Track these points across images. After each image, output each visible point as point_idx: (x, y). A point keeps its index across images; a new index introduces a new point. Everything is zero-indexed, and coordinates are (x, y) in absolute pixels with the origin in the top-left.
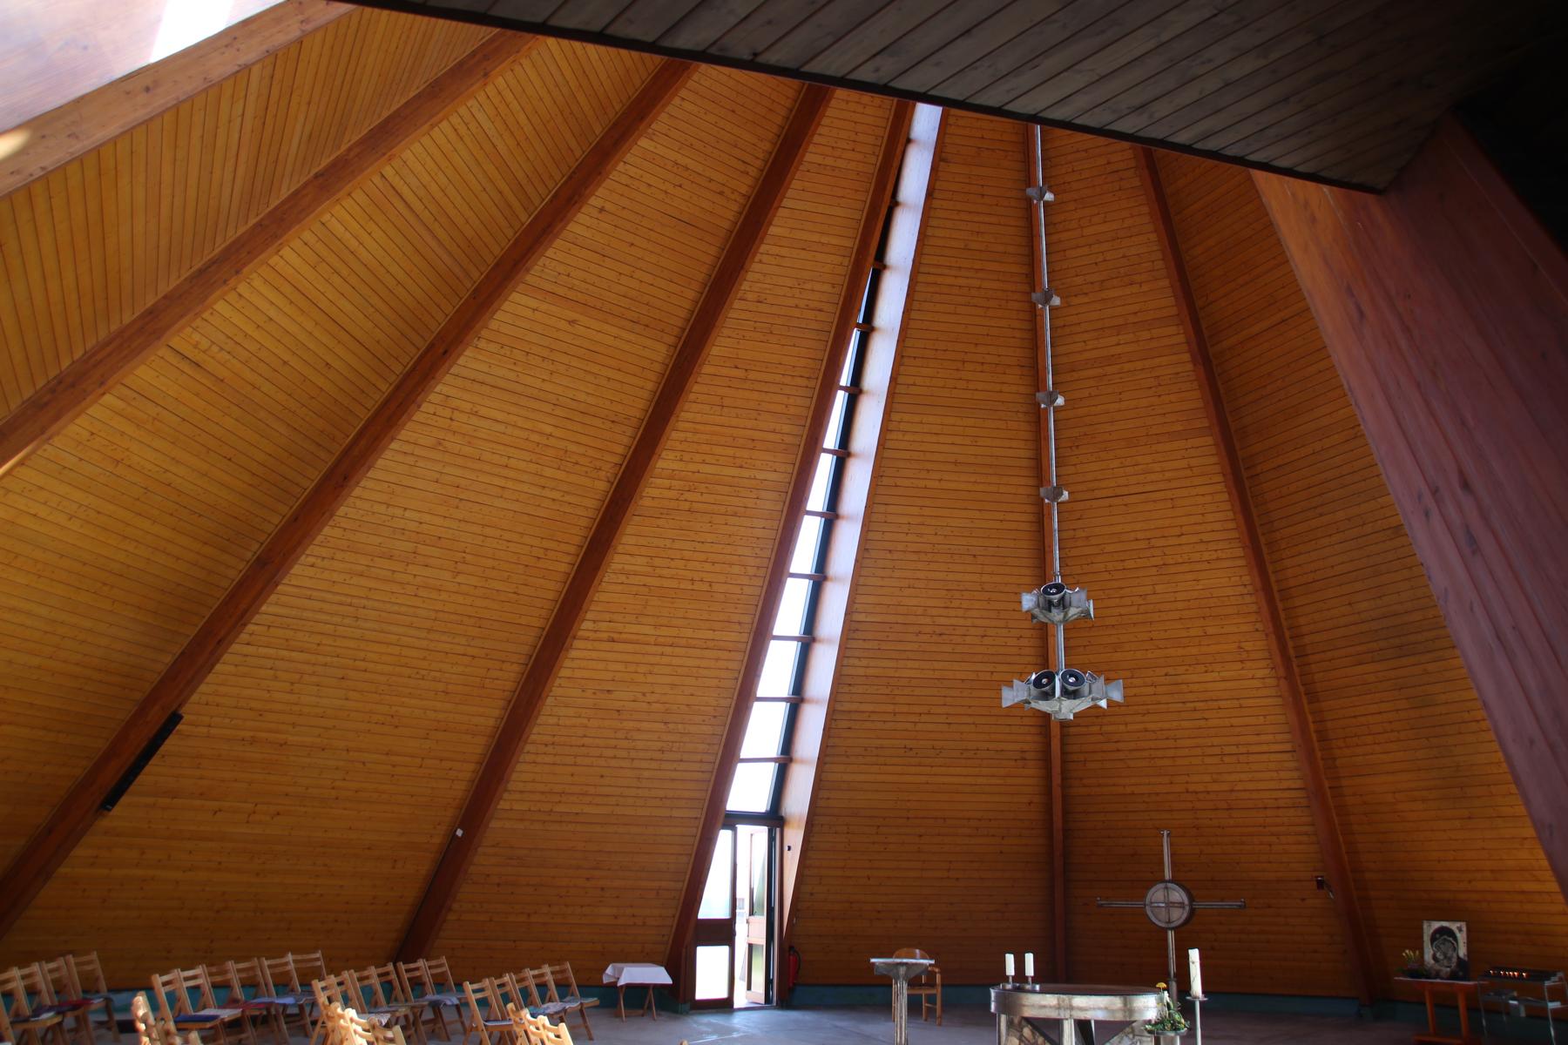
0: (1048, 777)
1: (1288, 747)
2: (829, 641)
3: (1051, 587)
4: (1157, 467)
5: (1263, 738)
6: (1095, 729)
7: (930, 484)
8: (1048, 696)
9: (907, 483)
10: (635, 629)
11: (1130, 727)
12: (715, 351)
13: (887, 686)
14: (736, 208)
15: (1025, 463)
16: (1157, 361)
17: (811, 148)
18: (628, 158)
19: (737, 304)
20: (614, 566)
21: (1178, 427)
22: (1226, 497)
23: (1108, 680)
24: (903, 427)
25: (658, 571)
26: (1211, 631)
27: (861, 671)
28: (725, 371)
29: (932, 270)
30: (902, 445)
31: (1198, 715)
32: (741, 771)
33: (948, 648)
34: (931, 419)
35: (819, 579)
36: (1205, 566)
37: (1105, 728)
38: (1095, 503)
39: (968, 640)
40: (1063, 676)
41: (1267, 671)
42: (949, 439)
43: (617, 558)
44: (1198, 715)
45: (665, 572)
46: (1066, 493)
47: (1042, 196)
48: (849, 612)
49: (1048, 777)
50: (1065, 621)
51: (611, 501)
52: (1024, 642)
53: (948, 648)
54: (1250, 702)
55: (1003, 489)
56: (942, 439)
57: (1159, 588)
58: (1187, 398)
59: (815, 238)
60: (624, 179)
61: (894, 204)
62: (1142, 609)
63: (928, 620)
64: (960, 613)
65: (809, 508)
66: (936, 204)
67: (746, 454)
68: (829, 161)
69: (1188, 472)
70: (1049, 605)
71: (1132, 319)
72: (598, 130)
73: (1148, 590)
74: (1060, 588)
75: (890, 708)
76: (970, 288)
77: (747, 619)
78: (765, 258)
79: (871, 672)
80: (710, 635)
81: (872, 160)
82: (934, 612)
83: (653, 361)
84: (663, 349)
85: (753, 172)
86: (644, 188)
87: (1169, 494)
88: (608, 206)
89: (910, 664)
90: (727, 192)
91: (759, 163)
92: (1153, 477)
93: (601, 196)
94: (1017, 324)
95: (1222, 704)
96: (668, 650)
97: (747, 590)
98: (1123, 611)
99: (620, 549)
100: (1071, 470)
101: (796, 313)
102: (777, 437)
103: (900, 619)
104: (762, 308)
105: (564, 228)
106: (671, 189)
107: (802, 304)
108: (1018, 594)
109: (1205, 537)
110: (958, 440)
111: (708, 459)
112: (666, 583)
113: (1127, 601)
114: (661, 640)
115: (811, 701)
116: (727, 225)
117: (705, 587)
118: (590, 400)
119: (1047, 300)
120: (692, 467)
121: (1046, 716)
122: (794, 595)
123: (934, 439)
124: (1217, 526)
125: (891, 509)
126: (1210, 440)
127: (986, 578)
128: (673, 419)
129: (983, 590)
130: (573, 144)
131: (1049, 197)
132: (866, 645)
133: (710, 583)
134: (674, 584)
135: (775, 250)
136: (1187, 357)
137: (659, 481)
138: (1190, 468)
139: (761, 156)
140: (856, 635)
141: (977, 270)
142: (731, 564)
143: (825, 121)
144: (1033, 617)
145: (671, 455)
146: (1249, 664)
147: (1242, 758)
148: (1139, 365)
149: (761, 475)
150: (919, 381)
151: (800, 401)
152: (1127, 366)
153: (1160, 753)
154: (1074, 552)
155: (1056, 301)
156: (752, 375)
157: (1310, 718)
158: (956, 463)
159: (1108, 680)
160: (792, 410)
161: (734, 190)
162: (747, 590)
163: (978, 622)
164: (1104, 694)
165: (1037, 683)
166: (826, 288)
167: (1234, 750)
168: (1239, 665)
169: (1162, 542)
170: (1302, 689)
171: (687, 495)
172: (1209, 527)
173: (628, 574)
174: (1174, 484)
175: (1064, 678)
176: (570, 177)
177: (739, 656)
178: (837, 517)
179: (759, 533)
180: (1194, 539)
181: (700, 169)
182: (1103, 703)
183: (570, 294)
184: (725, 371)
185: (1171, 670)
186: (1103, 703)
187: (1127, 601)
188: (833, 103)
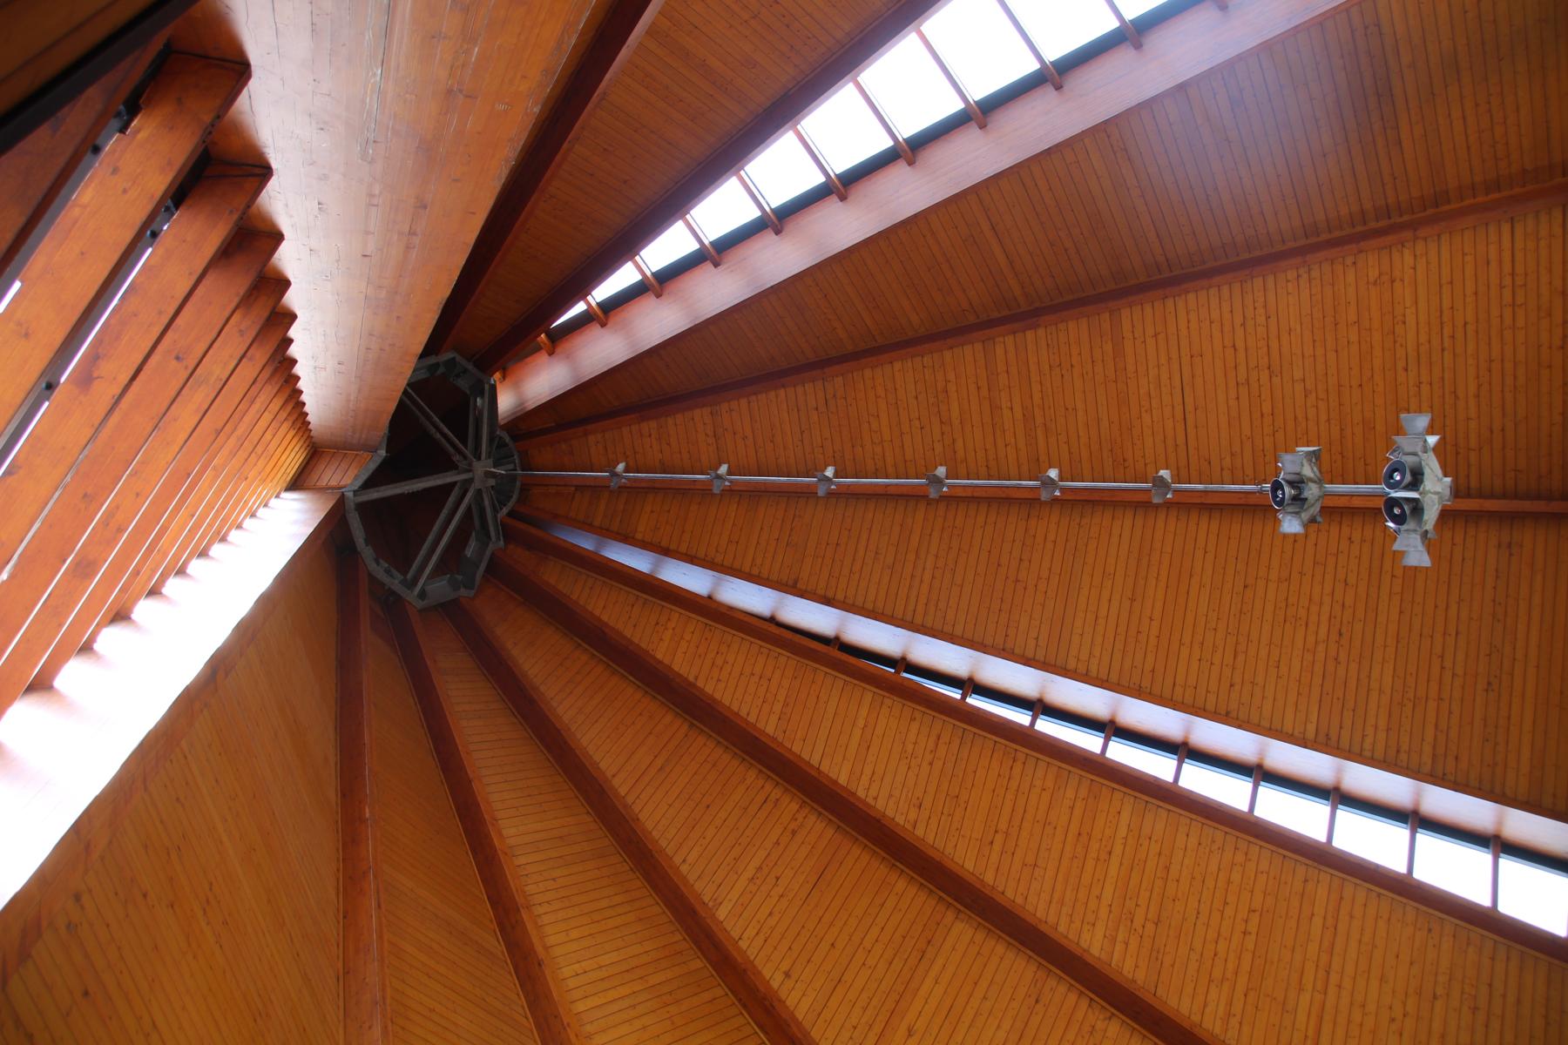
0: (1536, 517)
1: (1506, 228)
2: (1339, 771)
3: (1275, 496)
5: (1493, 255)
6: (1473, 457)
7: (1155, 632)
8: (1417, 508)
9: (1150, 658)
10: (1302, 1017)
11: (1473, 413)
12: (969, 865)
13: (1402, 705)
14: (813, 818)
15: (1139, 522)
16: (1033, 368)
17: (761, 725)
18: (735, 934)
19: (920, 832)
20: (1217, 1031)
21: (1108, 347)
22: (1191, 296)
23: (1399, 431)
25: (1229, 975)
26: (1353, 317)
27: (1382, 736)
28: (994, 857)
29: (911, 608)
30: (1106, 659)
31: (1459, 335)
32: (1422, 874)
33: (1358, 626)
34: (1078, 623)
35: (1183, 750)
36: (1273, 320)
37: (1473, 444)
39: (1349, 601)
40: (1391, 487)
41: (1406, 252)
43: (1207, 1024)
44: (1459, 335)
45: (1231, 966)
46: (1163, 473)
48: (1304, 743)
49: (1536, 517)
51: (1134, 1019)
52: (1357, 536)
53: (1358, 626)
54: (1446, 272)
56: (1103, 613)
57: (1298, 375)
58: (1076, 332)
59: (857, 733)
61: (772, 620)
62: (1322, 395)
63: (1321, 648)
64: (1314, 609)
65: (1098, 751)
66: (840, 596)
67: (1095, 846)
68: (778, 707)
69: (1162, 337)
70: (1298, 500)
71: (984, 392)
72: (698, 964)
73: (1299, 387)
74: (1277, 486)
75: (1432, 705)
76: (935, 567)
77: (1301, 870)
78: (873, 792)
79: (1382, 723)
80: (1318, 921)
81: (783, 660)
82: (1311, 639)
83: (972, 941)
84: (960, 926)
85: (777, 793)
86: (772, 921)
87: (1186, 360)
88: (785, 966)
90: (793, 826)
91: (769, 787)
92: (1165, 376)
93: (772, 974)
94: (981, 519)
95: (1446, 303)
96: (1334, 978)
97: (1264, 866)
98: (1323, 417)
99: (1196, 1018)
101: (938, 765)
102: (1079, 805)
103: (1317, 680)
105: (799, 1024)
106: (780, 890)
107: (929, 757)
108: (1285, 536)
109: (1238, 320)
110: (1106, 594)
111: (1096, 892)
112: (1246, 966)
113: (1312, 413)
114: (1319, 985)
115: (1417, 803)
116: (830, 831)
117: (1255, 918)
118: (1006, 1026)
119: (938, 481)
120: (1104, 911)
121: (1445, 515)
122: (1200, 781)
123: (1101, 621)
124: (1226, 307)
125: (1180, 680)
126: (1125, 313)
127: (1274, 575)
128: (1043, 928)
129: (1289, 579)
130: (706, 996)
131: (829, 472)
132: (1347, 722)
134: (1247, 957)
135: (865, 779)
136: (1030, 334)
137: (1116, 956)
139: (761, 782)
140: (1334, 738)
142: (1229, 882)
143: (735, 708)
144: (1313, 520)
145: (1086, 936)
146: (1397, 274)
147: (1519, 281)
148: (1036, 388)
149: (1122, 832)
150: (1033, 634)
151: (1040, 773)
153: (1509, 381)
154: (1249, 471)
155: (941, 471)
156: (1003, 826)
157: (1467, 202)
158: (1132, 600)
160: (1049, 784)
161: (794, 819)
162: (1264, 866)
163: (1328, 589)
164: (1420, 439)
165: (1399, 520)
166: (915, 726)
167: (1507, 293)
168: (1397, 284)
169: (1242, 369)
170: (1430, 211)
172: (1227, 316)
173: (1229, 1015)
174: (1174, 355)
176: (744, 1006)
177: (1349, 890)
178: (1112, 722)
179: (1193, 840)
180: (1240, 332)
181: (762, 854)
182: (1432, 440)
183: (877, 1029)
184: (994, 857)
185: (1401, 364)
186: (1432, 440)
187: (1312, 413)
188: (717, 696)
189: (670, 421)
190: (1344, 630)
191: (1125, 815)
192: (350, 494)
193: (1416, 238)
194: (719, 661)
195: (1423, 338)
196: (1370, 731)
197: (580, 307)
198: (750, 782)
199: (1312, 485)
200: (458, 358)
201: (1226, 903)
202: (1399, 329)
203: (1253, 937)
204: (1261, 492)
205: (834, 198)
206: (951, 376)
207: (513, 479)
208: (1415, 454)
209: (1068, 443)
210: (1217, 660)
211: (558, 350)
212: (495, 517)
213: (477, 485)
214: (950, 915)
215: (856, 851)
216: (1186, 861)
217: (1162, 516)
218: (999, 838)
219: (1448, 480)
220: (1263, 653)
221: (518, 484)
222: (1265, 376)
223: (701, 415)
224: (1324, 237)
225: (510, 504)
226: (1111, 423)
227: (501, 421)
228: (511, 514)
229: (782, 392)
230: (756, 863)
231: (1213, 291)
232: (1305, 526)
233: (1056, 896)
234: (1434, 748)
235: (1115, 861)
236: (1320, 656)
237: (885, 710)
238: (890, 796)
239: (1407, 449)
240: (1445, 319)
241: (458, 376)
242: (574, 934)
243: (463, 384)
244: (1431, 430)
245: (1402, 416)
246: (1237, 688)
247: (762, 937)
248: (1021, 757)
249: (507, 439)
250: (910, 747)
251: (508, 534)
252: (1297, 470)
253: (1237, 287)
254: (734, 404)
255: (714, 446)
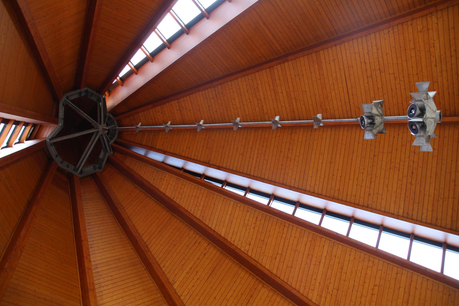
4: (334, 75)
7: (339, 175)
8: (423, 126)
14: (212, 249)
16: (289, 77)
21: (316, 66)
22: (346, 44)
23: (416, 90)
24: (312, 185)
26: (412, 46)
27: (430, 213)
28: (276, 264)
29: (249, 169)
34: (310, 172)
38: (351, 101)
39: (416, 160)
41: (433, 17)
42: (320, 165)
47: (201, 125)
50: (381, 115)
55: (344, 142)
56: (319, 168)
57: (391, 72)
59: (228, 217)
60: (188, 297)
62: (401, 79)
63: (405, 179)
64: (402, 163)
67: (314, 259)
68: (201, 208)
69: (336, 61)
71: (272, 87)
73: (392, 76)
75: (451, 200)
76: (258, 154)
77: (395, 269)
78: (233, 239)
79: (430, 209)
80: (402, 290)
82: (401, 176)
83: (268, 296)
84: (263, 290)
85: (200, 239)
89: (427, 189)
90: (205, 252)
97: (380, 267)
98: (403, 88)
100: (336, 112)
101: (257, 228)
102: (309, 244)
103: (403, 192)
104: (252, 243)
106: (197, 277)
107: (253, 226)
110: (321, 161)
111: (314, 277)
113: (398, 86)
115: (446, 240)
117: (376, 288)
119: (275, 122)
120: (317, 284)
121: (440, 126)
123: (319, 172)
125: (349, 193)
126: (321, 52)
127: (385, 151)
129: (391, 152)
131: (277, 118)
132: (416, 208)
133: (375, 285)
135: (230, 235)
136: (286, 64)
138: (334, 60)
140: (410, 213)
141: (251, 150)
142: (366, 274)
146: (430, 27)
148: (290, 84)
149: (325, 254)
152: (291, 89)
156: (280, 252)
158: (331, 163)
159: (416, 90)
160: (297, 235)
161: (205, 249)
162: (380, 267)
163: (407, 155)
165: (415, 131)
166: (248, 214)
168: (430, 31)
171: (330, 290)
175: (412, 116)
179: (352, 257)
182: (432, 94)
185: (433, 64)
186: (432, 94)
187: (398, 86)
189: (165, 106)
190: (414, 172)
191: (326, 247)
192: (48, 140)
193: (437, 11)
194: (181, 191)
195: (442, 52)
196: (425, 211)
197: (126, 69)
198: (191, 235)
199: (377, 117)
200: (89, 89)
201: (365, 282)
202: (432, 49)
203: (376, 296)
204: (357, 121)
205: (205, 19)
206: (259, 82)
207: (116, 130)
208: (421, 101)
209: (304, 104)
210: (363, 185)
211: (124, 84)
212: (109, 144)
213: (101, 133)
214: (260, 286)
215: (227, 261)
216: (349, 266)
217: (342, 130)
218: (278, 257)
219: (439, 111)
220: (382, 181)
221: (117, 132)
222: (378, 73)
223: (174, 103)
224: (398, 14)
225: (114, 139)
226: (320, 96)
227: (108, 110)
228: (116, 142)
229: (200, 93)
230: (190, 266)
231: (355, 41)
232: (375, 135)
233: (299, 279)
234: (452, 217)
235: (322, 265)
236: (405, 182)
237: (238, 208)
238: (239, 240)
239: (417, 98)
240: (451, 44)
241: (91, 96)
242: (114, 298)
243: (94, 99)
244: (430, 89)
245: (417, 83)
246: (372, 195)
247: (189, 295)
248: (287, 225)
249: (111, 116)
250: (246, 222)
251: (114, 149)
252: (370, 111)
253: (364, 38)
254: (185, 98)
255: (168, 116)
